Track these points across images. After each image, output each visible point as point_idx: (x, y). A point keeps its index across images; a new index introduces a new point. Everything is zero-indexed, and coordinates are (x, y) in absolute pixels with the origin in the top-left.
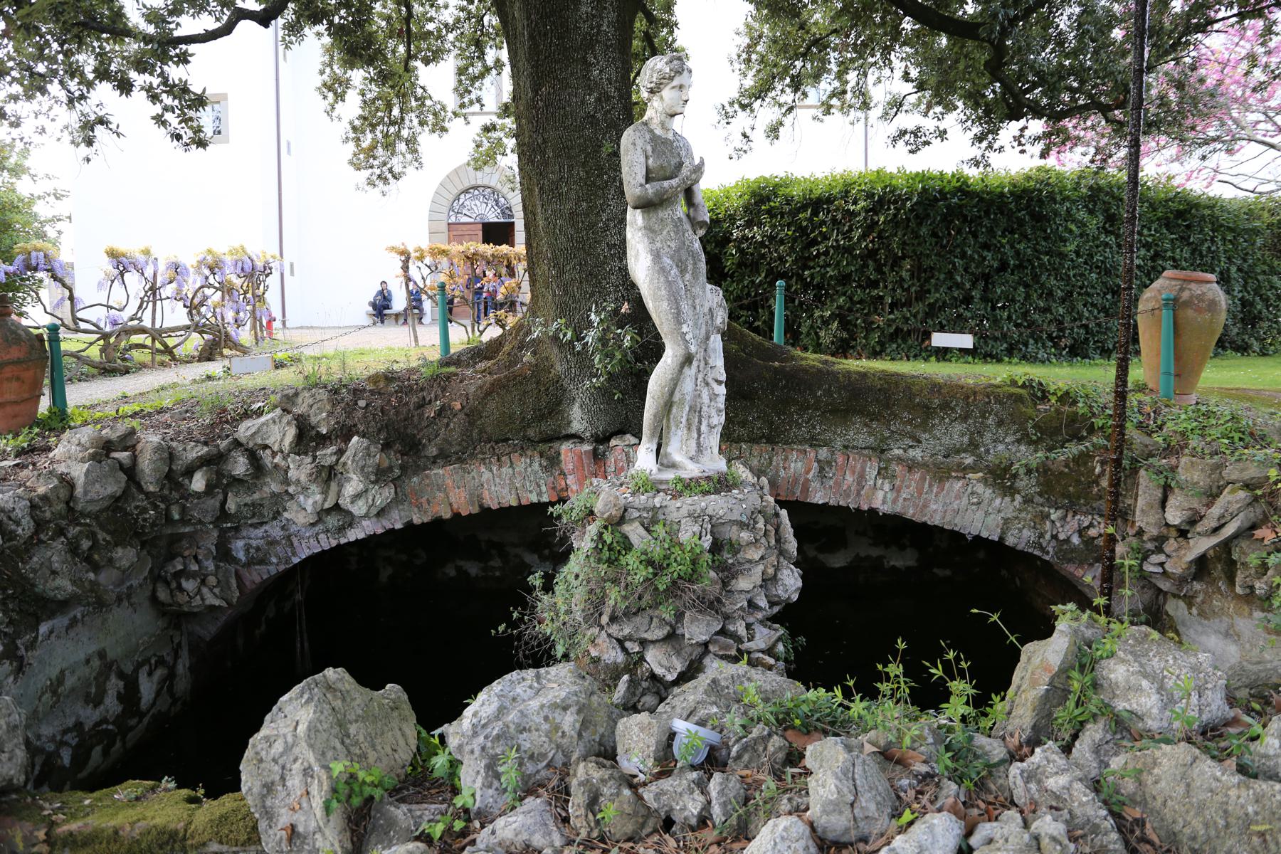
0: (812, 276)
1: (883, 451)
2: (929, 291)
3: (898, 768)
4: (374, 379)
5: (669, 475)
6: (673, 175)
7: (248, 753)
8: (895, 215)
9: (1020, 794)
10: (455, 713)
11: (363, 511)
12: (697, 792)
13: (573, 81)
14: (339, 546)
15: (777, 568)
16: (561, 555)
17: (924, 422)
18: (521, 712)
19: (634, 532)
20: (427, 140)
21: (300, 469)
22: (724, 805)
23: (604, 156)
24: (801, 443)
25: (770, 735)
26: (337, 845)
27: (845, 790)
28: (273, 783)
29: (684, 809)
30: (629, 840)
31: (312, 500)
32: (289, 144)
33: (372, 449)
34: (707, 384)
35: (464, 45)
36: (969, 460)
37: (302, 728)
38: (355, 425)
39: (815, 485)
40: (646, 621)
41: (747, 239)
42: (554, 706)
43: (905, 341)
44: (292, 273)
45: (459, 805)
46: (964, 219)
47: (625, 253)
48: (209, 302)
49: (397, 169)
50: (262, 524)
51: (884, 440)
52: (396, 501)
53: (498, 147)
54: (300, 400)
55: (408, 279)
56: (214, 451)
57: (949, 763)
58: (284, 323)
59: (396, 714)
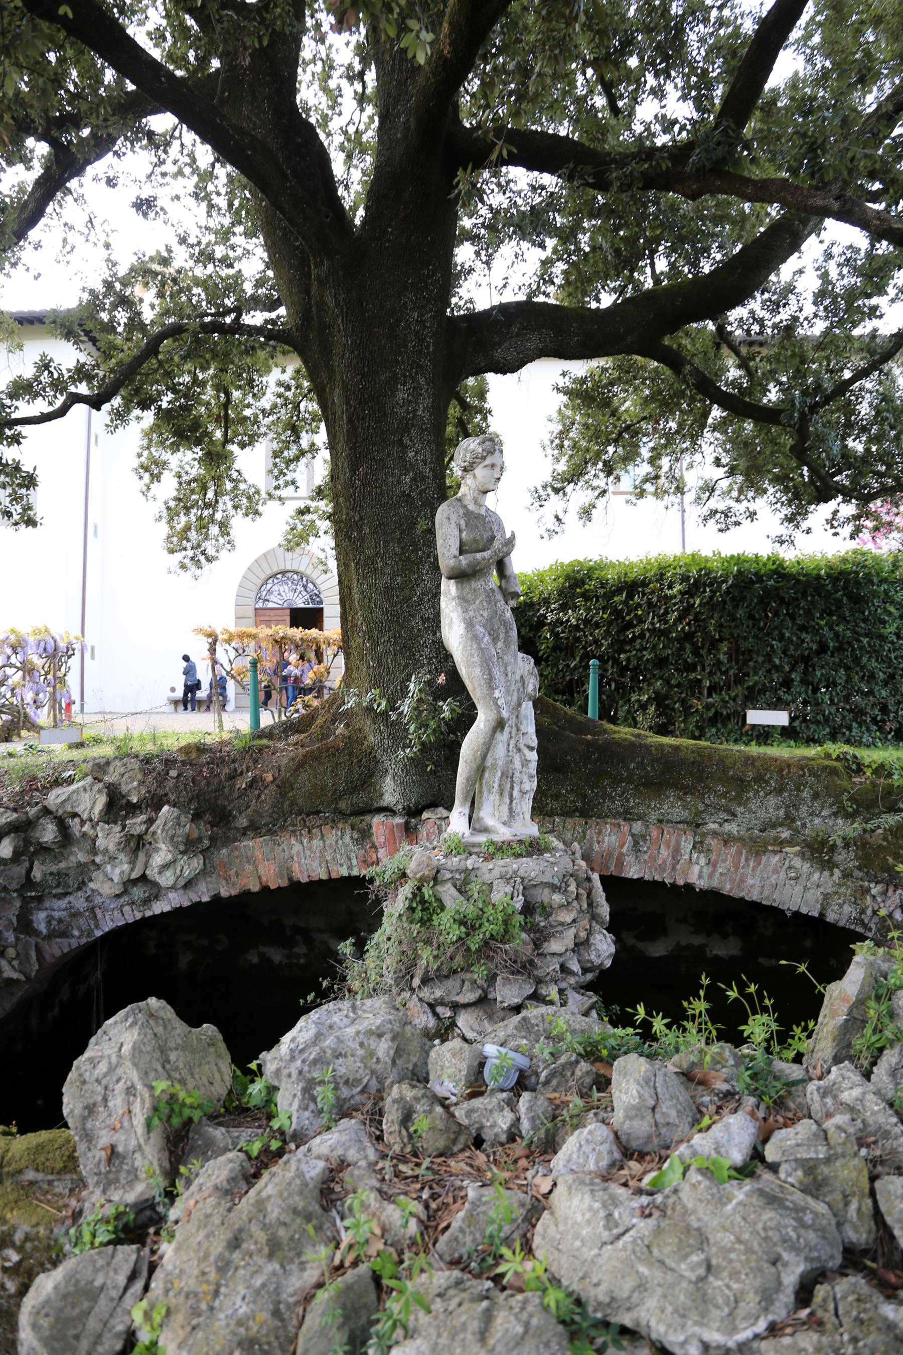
0: (628, 659)
1: (698, 826)
2: (747, 674)
3: (700, 1088)
4: (186, 750)
5: (482, 838)
6: (487, 551)
7: (72, 1076)
8: (711, 598)
9: (816, 1107)
10: (271, 1042)
11: (171, 882)
12: (507, 1109)
13: (389, 462)
14: (143, 919)
15: (590, 933)
16: (374, 920)
17: (739, 797)
18: (338, 1038)
19: (448, 893)
20: (239, 523)
21: (108, 838)
22: (532, 1120)
23: (418, 532)
24: (614, 817)
25: (577, 1062)
26: (156, 1164)
27: (647, 1095)
28: (94, 1104)
29: (494, 1125)
30: (440, 1155)
31: (120, 870)
32: (96, 527)
33: (182, 818)
34: (519, 750)
35: (280, 430)
36: (786, 834)
37: (126, 1049)
38: (166, 795)
39: (629, 859)
40: (459, 982)
41: (562, 623)
42: (369, 1033)
43: (725, 725)
44: (93, 657)
45: (276, 1127)
46: (782, 601)
47: (439, 627)
48: (10, 682)
49: (211, 551)
50: (66, 894)
51: (698, 813)
52: (205, 872)
53: (311, 530)
54: (111, 769)
55: (215, 662)
56: (24, 818)
57: (748, 1080)
58: (82, 706)
59: (212, 1050)
